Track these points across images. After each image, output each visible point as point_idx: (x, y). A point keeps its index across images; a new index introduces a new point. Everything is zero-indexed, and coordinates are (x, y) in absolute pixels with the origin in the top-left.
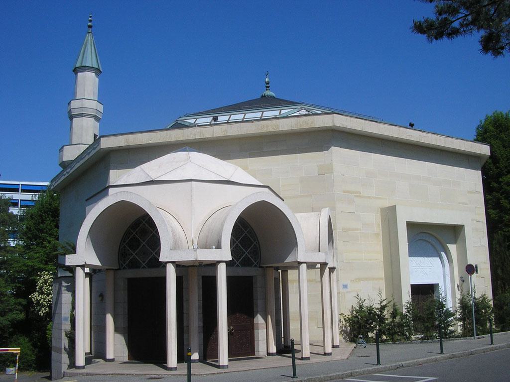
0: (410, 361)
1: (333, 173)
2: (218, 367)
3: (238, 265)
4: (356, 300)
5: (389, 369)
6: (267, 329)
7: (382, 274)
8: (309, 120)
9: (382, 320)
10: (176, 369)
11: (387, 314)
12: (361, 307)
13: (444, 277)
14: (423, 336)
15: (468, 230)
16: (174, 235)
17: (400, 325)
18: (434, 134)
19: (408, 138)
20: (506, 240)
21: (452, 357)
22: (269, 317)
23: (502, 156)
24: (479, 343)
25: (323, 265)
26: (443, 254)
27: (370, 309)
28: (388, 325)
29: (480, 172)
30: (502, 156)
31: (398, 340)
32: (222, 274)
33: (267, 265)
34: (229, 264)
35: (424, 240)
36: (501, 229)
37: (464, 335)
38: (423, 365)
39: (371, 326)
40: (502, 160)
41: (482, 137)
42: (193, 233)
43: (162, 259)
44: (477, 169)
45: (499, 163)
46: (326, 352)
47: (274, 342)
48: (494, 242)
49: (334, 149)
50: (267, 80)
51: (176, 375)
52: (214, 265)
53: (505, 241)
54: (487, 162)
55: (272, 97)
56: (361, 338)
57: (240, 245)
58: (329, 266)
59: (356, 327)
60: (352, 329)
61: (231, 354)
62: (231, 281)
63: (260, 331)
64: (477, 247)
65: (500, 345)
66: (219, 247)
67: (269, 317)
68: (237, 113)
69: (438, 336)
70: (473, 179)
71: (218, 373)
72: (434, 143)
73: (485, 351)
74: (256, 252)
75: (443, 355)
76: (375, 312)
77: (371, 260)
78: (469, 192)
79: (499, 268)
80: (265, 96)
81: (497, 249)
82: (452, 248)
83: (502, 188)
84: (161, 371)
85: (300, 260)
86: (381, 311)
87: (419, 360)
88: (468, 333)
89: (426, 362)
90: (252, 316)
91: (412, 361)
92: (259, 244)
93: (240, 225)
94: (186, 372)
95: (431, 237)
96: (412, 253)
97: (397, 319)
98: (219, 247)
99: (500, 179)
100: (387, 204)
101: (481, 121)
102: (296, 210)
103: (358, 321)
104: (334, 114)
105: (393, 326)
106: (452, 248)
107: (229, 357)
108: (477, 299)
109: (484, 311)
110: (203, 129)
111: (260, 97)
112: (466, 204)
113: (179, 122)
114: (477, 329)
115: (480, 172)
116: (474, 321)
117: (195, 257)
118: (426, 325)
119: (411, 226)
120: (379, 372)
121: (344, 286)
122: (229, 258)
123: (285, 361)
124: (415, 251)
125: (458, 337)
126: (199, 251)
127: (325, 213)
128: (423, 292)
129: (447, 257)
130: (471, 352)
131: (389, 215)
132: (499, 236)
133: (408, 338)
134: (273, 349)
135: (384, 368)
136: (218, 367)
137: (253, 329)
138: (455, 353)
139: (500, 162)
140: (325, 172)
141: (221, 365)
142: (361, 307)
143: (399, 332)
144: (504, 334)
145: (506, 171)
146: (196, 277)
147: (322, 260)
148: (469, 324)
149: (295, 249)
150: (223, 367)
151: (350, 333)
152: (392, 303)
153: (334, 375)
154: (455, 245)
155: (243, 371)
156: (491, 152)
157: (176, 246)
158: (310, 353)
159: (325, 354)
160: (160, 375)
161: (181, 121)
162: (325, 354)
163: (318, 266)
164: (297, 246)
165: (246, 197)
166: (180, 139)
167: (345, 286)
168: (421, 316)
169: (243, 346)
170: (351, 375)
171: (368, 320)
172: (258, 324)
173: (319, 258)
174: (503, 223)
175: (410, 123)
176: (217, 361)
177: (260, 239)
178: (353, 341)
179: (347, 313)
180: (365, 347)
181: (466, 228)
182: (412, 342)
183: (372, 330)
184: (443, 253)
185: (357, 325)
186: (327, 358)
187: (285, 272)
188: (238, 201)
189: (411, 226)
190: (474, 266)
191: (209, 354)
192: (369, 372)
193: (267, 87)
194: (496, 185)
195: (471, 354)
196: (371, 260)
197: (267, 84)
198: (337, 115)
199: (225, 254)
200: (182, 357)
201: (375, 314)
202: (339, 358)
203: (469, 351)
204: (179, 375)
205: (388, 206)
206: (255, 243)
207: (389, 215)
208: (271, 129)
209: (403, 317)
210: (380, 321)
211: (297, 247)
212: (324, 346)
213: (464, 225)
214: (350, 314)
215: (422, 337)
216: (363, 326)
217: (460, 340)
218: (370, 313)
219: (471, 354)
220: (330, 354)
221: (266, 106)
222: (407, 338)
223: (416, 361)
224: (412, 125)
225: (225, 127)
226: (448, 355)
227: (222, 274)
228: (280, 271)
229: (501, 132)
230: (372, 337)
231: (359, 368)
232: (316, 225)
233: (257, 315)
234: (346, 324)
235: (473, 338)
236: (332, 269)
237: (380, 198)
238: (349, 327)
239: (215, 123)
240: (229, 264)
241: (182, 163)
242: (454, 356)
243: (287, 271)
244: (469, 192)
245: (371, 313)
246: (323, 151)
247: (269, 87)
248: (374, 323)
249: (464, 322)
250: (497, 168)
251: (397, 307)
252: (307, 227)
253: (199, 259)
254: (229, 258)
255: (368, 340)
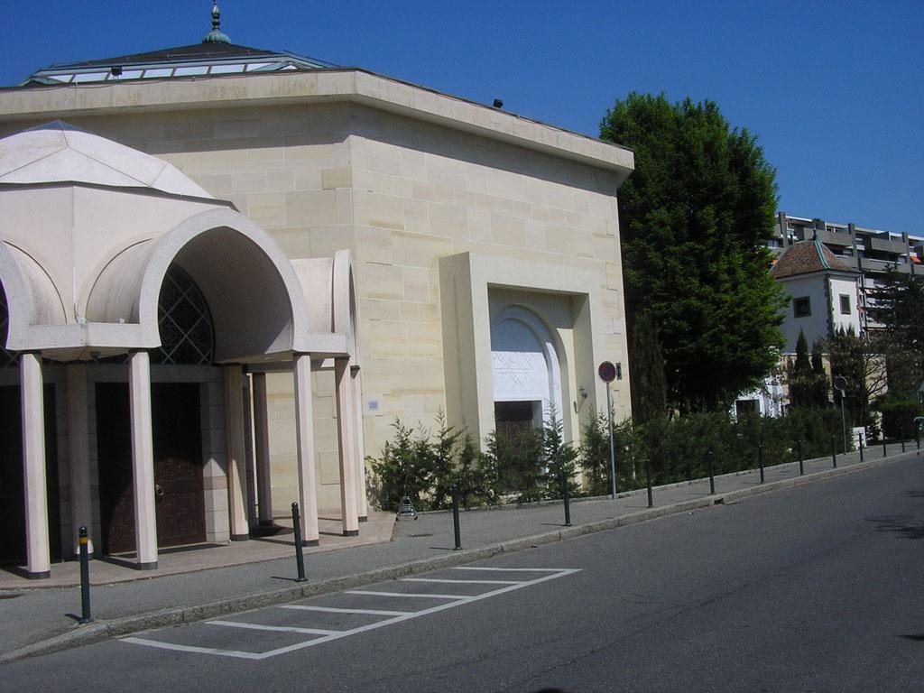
0: (515, 541)
1: (351, 186)
2: (138, 567)
3: (169, 362)
4: (395, 431)
5: (479, 557)
6: (229, 488)
7: (440, 382)
8: (306, 81)
9: (443, 467)
10: (47, 575)
11: (455, 454)
12: (404, 444)
13: (551, 389)
14: (520, 495)
15: (594, 304)
16: (37, 298)
17: (478, 476)
18: (539, 123)
19: (493, 128)
20: (657, 324)
21: (587, 530)
22: (234, 463)
23: (650, 173)
24: (629, 505)
25: (341, 359)
26: (549, 346)
27: (423, 448)
28: (455, 476)
29: (615, 200)
30: (650, 173)
31: (474, 504)
32: (141, 376)
33: (227, 361)
34: (154, 355)
35: (516, 320)
36: (647, 304)
37: (594, 493)
38: (539, 547)
39: (423, 480)
40: (650, 181)
41: (615, 133)
42: (76, 292)
43: (12, 344)
44: (609, 193)
45: (644, 186)
46: (348, 530)
47: (244, 514)
48: (635, 328)
49: (354, 140)
50: (215, 9)
51: (50, 587)
52: (122, 358)
53: (654, 327)
54: (624, 184)
55: (224, 43)
56: (407, 502)
57: (173, 321)
58: (352, 362)
59: (394, 481)
60: (387, 487)
61: (162, 541)
62: (159, 392)
63: (215, 492)
64: (609, 333)
65: (665, 507)
66: (133, 318)
67: (234, 463)
68: (158, 66)
69: (549, 495)
70: (602, 211)
71: (137, 579)
72: (538, 139)
73: (641, 518)
74: (207, 336)
75: (571, 528)
76: (431, 453)
77: (421, 355)
78: (597, 235)
79: (644, 374)
80: (210, 41)
81: (641, 341)
82: (566, 335)
83: (649, 231)
84: (17, 582)
85: (298, 348)
86: (442, 451)
87: (531, 538)
88: (600, 488)
89: (546, 541)
90: (198, 462)
91: (518, 541)
92: (212, 321)
93: (173, 281)
94: (76, 578)
95: (530, 315)
96: (497, 344)
97: (474, 466)
98: (133, 318)
99: (648, 215)
100: (451, 249)
101: (608, 111)
102: (293, 253)
103: (399, 471)
104: (357, 72)
105: (465, 476)
106: (566, 335)
107: (158, 547)
108: (617, 426)
109: (627, 449)
110: (92, 91)
111: (200, 42)
112: (592, 257)
113: (36, 80)
114: (619, 482)
115: (616, 199)
116: (613, 465)
117: (84, 341)
118: (527, 475)
119: (496, 292)
120: (462, 563)
121: (370, 404)
122: (155, 342)
123: (278, 552)
124: (503, 339)
125: (584, 495)
126: (92, 326)
127: (342, 259)
128: (515, 415)
129: (556, 352)
130: (619, 520)
131: (456, 270)
132: (644, 318)
133: (493, 501)
134: (243, 527)
135: (469, 555)
136: (138, 567)
137: (202, 489)
138: (591, 524)
139: (648, 185)
140: (337, 184)
141: (307, 539)
142: (404, 444)
143: (477, 488)
144: (662, 490)
145: (657, 202)
146: (89, 382)
147: (340, 349)
148: (604, 471)
149: (287, 327)
150: (147, 566)
151: (383, 494)
152: (463, 436)
153: (378, 573)
154: (571, 330)
155: (191, 572)
156: (636, 166)
157: (41, 317)
158: (320, 533)
159: (346, 533)
160: (14, 588)
161: (41, 77)
162: (346, 533)
163: (330, 363)
164: (292, 319)
165: (190, 218)
166: (41, 110)
167: (374, 405)
168: (516, 458)
169: (184, 523)
170: (410, 571)
171: (417, 468)
172: (211, 478)
173: (336, 344)
174: (652, 294)
175: (495, 101)
176: (134, 556)
177: (218, 311)
178: (389, 507)
179: (378, 456)
180: (416, 519)
181: (592, 301)
182: (500, 507)
183: (425, 486)
184: (550, 344)
185: (398, 479)
186: (350, 542)
187: (260, 376)
188: (166, 232)
189: (496, 292)
190: (615, 366)
191: (115, 537)
192: (444, 564)
193: (215, 24)
194: (639, 225)
195: (619, 525)
196: (421, 355)
197: (215, 18)
198: (362, 73)
199: (148, 334)
200: (59, 552)
201: (431, 456)
202: (373, 539)
203: (616, 518)
204: (57, 587)
205: (453, 254)
206: (203, 316)
207: (456, 270)
208: (230, 96)
209: (484, 460)
210: (441, 469)
211: (292, 322)
212: (343, 520)
213: (588, 294)
214: (382, 457)
215: (519, 498)
216: (405, 479)
217: (588, 502)
218: (421, 455)
219: (619, 524)
220: (355, 533)
221: (213, 56)
222: (491, 499)
223: (525, 539)
224: (498, 104)
225: (135, 87)
226: (580, 527)
227: (141, 376)
228: (250, 375)
229: (649, 130)
230: (426, 500)
231: (422, 558)
232: (327, 282)
233: (208, 460)
234: (375, 475)
235: (610, 496)
236: (355, 370)
237: (437, 239)
238: (381, 483)
239: (116, 78)
240: (154, 355)
241: (50, 150)
242: (591, 530)
243: (264, 374)
244: (597, 235)
245: (424, 455)
246: (332, 143)
247: (218, 24)
248: (430, 474)
249: (594, 469)
250: (642, 194)
251: (471, 442)
252: (310, 285)
253: (94, 345)
254: (155, 342)
255: (419, 505)
